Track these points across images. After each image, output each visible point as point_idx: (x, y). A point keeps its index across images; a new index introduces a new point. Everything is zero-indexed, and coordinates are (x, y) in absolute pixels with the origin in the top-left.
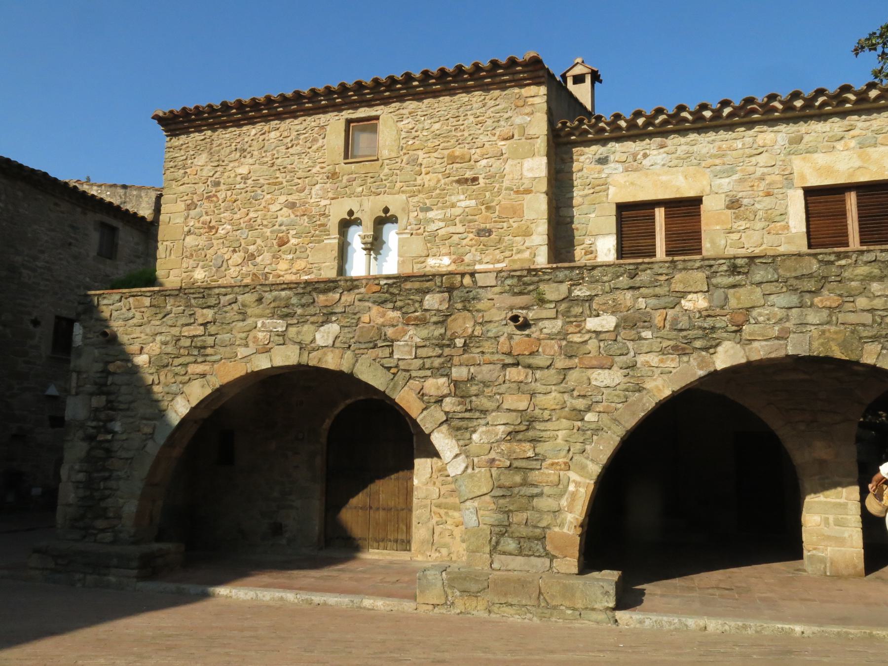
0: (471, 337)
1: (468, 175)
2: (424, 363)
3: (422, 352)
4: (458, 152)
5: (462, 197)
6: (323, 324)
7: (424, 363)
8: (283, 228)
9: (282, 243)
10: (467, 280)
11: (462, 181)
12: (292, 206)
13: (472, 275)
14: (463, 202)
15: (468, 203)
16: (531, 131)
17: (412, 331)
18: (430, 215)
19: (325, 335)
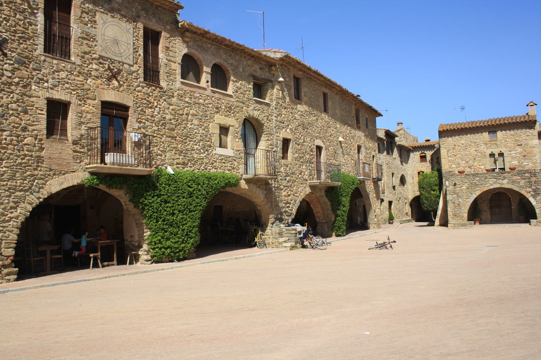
0: (535, 181)
1: (519, 144)
2: (67, 53)
3: (525, 184)
4: (517, 139)
5: (519, 149)
6: (504, 180)
7: (67, 53)
8: (474, 156)
9: (475, 159)
10: (534, 171)
11: (519, 145)
12: (476, 151)
13: (535, 170)
14: (519, 149)
15: (520, 150)
16: (534, 134)
17: (523, 180)
18: (512, 152)
19: (505, 181)
